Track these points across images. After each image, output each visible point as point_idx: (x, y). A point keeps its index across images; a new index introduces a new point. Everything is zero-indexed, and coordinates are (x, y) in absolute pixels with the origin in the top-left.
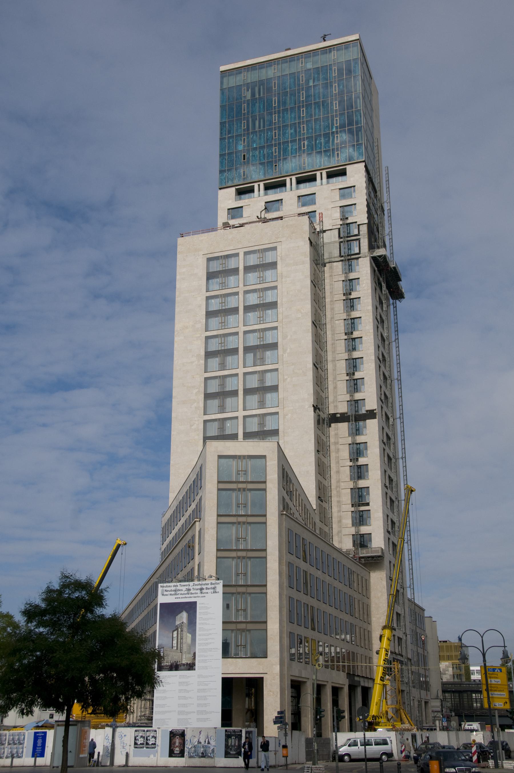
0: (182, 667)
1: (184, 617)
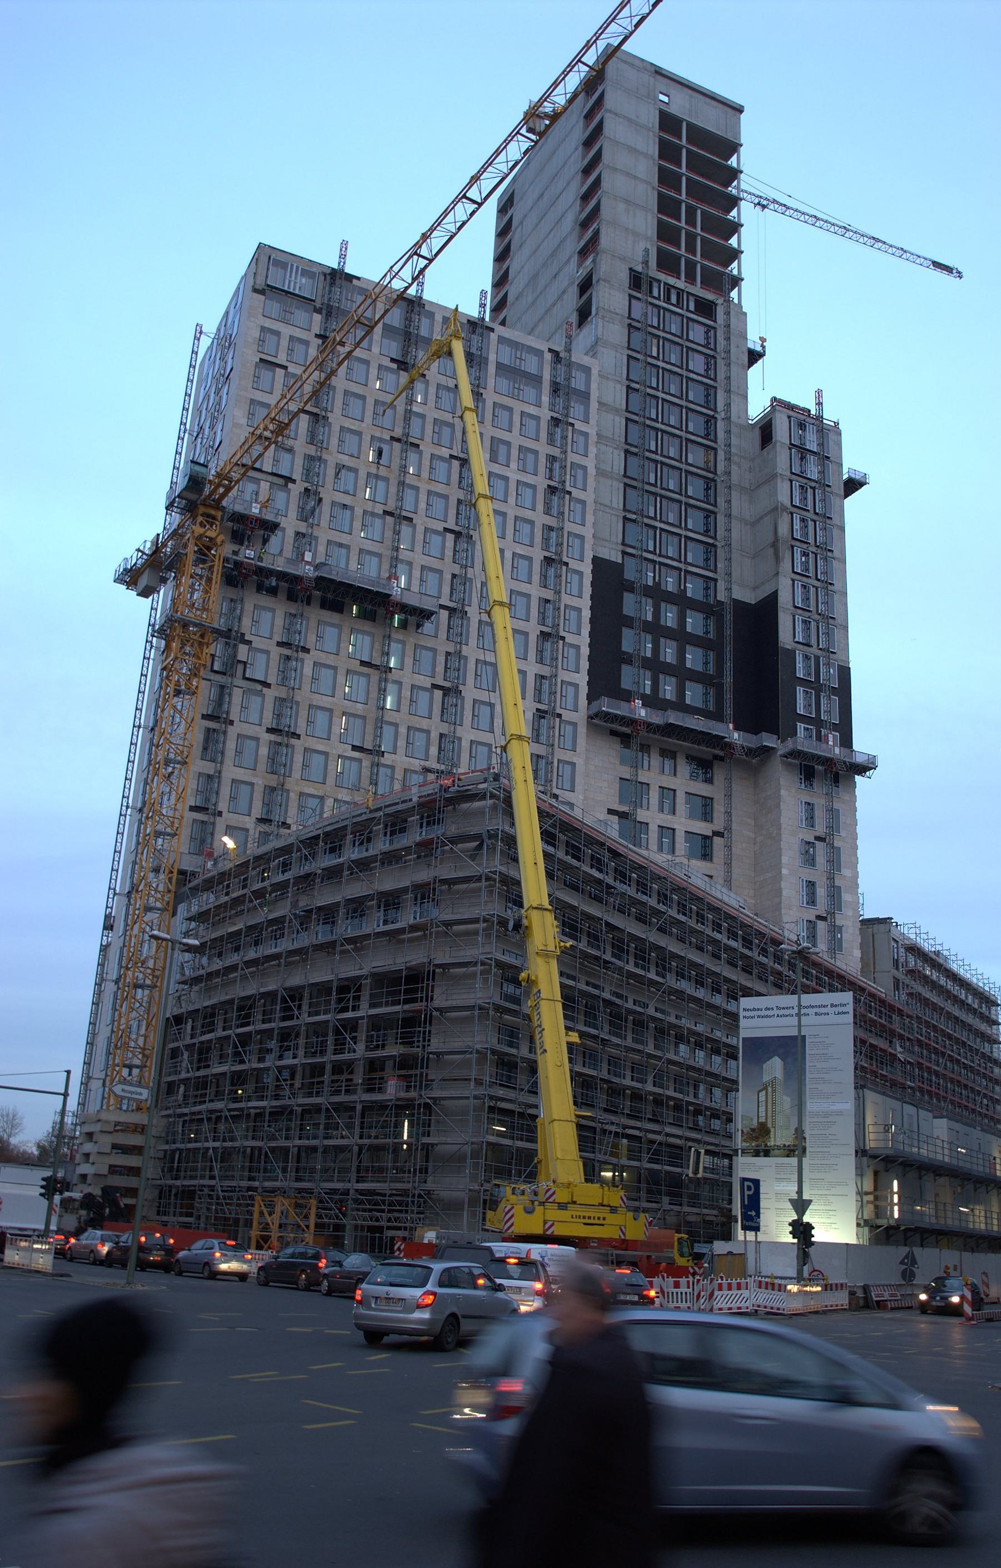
1: (775, 1067)
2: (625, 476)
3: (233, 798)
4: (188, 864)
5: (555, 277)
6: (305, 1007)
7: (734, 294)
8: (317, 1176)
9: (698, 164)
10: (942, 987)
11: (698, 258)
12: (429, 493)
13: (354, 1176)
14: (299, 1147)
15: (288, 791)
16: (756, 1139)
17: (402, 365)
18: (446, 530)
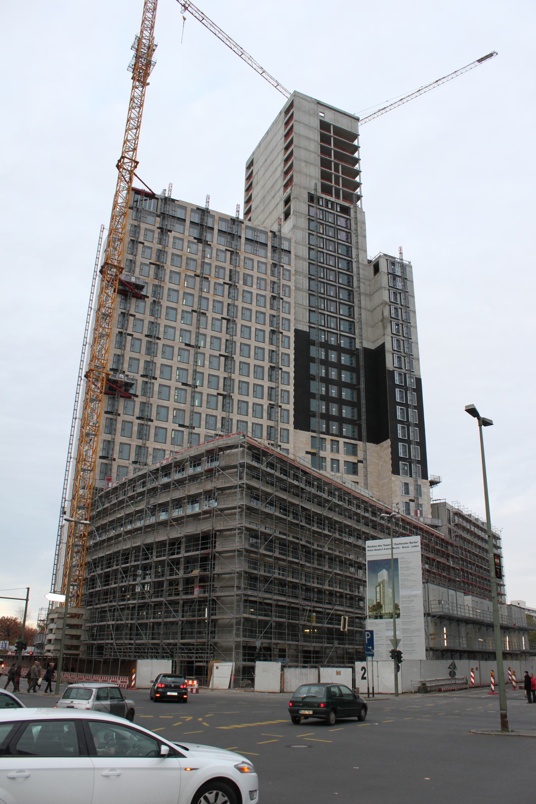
0: (386, 616)
1: (384, 574)
2: (309, 290)
3: (121, 452)
4: (99, 484)
5: (273, 197)
6: (154, 554)
7: (359, 203)
8: (161, 636)
9: (338, 144)
10: (472, 531)
11: (341, 187)
12: (214, 301)
13: (179, 636)
14: (153, 623)
15: (148, 448)
16: (376, 610)
17: (199, 240)
18: (223, 318)
